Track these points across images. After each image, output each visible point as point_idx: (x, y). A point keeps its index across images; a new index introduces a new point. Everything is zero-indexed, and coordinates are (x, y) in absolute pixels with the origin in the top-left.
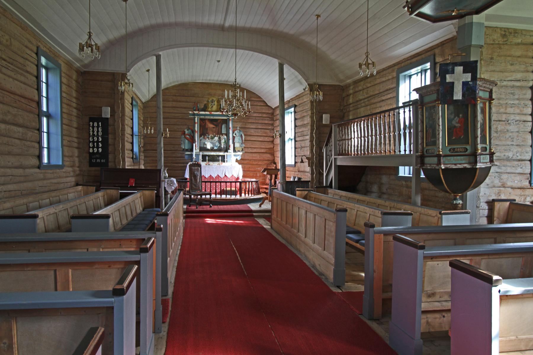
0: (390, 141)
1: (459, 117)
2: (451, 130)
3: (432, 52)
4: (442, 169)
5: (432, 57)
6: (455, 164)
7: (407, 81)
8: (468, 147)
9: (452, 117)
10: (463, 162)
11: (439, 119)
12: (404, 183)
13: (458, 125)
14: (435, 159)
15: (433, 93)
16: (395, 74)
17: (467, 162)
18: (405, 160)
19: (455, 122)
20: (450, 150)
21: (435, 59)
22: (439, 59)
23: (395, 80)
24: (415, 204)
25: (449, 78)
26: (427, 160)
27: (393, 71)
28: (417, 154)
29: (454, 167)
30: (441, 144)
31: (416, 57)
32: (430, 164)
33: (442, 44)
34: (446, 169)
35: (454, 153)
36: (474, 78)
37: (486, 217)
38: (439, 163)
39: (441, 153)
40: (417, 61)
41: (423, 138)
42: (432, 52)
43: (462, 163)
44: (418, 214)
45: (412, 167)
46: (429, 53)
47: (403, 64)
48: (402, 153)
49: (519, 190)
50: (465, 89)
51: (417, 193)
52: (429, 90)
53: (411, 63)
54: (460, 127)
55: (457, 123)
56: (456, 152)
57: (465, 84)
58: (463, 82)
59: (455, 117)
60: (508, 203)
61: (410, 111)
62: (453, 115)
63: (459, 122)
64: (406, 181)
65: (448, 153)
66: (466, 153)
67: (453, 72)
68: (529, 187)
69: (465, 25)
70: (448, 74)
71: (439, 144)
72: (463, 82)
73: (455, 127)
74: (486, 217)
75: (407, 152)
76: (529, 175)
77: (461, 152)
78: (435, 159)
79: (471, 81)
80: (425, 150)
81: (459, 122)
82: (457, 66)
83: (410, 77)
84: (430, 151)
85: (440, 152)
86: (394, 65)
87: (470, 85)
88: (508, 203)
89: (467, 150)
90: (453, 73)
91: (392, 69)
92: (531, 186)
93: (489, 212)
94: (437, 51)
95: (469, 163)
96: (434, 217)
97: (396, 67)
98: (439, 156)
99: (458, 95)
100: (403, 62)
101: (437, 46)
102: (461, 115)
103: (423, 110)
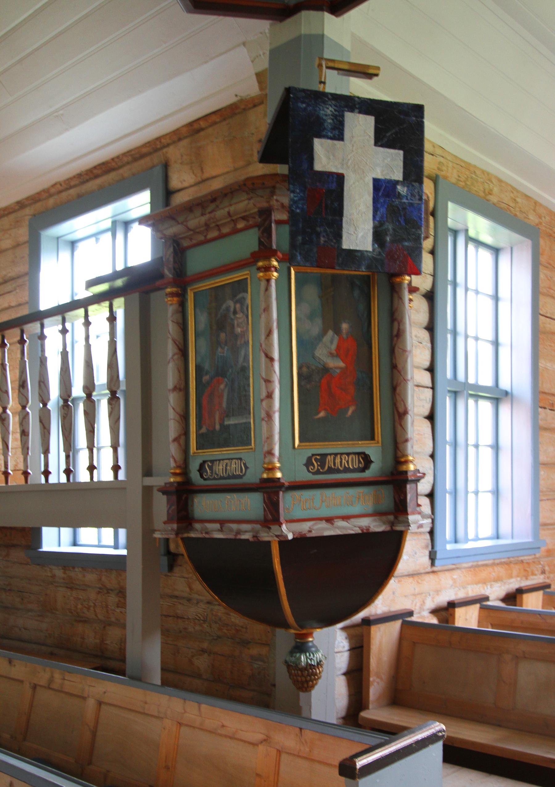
0: (24, 433)
1: (337, 331)
2: (314, 385)
3: (157, 158)
4: (284, 544)
5: (158, 171)
6: (329, 520)
7: (65, 254)
8: (373, 450)
9: (315, 328)
10: (357, 509)
11: (269, 333)
12: (59, 573)
13: (336, 364)
14: (252, 504)
15: (235, 231)
16: (23, 233)
17: (370, 510)
18: (80, 504)
19: (326, 353)
20: (308, 463)
21: (166, 179)
22: (181, 178)
23: (25, 251)
24: (138, 679)
25: (361, 126)
26: (204, 505)
27: (17, 223)
28: (157, 481)
29: (328, 531)
30: (277, 437)
31: (97, 177)
32: (222, 522)
33: (194, 129)
34: (301, 541)
35: (322, 478)
36: (414, 170)
37: (344, 674)
38: (272, 517)
39: (279, 475)
40: (101, 187)
41: (185, 417)
42: (157, 158)
43: (348, 513)
44: (168, 723)
45: (122, 532)
46: (145, 162)
47: (51, 202)
48: (57, 477)
49: (411, 580)
50: (382, 210)
51: (146, 633)
52: (220, 213)
53: (79, 196)
54: (344, 371)
55: (331, 355)
56: (331, 471)
57: (382, 190)
58: (377, 182)
59: (324, 332)
60: (397, 624)
61: (112, 319)
62: (319, 321)
63: (338, 353)
64: (65, 568)
65: (305, 476)
66: (368, 474)
67: (338, 133)
68: (429, 569)
69: (298, 39)
70: (320, 136)
71: (270, 437)
72: (377, 182)
73: (326, 370)
74: (344, 674)
75: (105, 474)
76: (428, 536)
77: (347, 470)
78: (252, 504)
79: (403, 183)
80: (194, 466)
81: (338, 353)
82: (352, 110)
83: (73, 244)
84: (219, 468)
85: (272, 469)
86: (21, 205)
87: (399, 196)
88: (397, 624)
89: (367, 461)
90: (340, 137)
91: (12, 217)
92: (433, 564)
93: (351, 657)
94: (173, 153)
95: (378, 514)
96: (254, 744)
97: (28, 211)
98: (270, 489)
99: (358, 231)
100: (51, 196)
101: (176, 136)
102: (345, 326)
103: (182, 305)
